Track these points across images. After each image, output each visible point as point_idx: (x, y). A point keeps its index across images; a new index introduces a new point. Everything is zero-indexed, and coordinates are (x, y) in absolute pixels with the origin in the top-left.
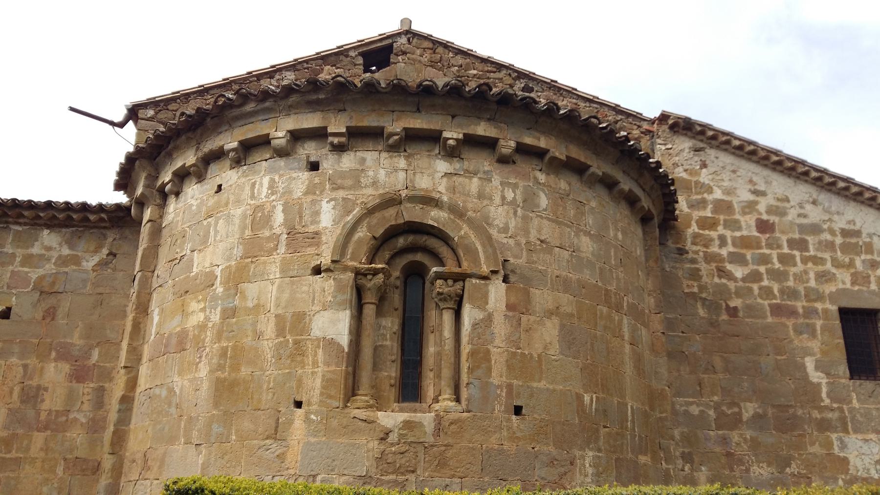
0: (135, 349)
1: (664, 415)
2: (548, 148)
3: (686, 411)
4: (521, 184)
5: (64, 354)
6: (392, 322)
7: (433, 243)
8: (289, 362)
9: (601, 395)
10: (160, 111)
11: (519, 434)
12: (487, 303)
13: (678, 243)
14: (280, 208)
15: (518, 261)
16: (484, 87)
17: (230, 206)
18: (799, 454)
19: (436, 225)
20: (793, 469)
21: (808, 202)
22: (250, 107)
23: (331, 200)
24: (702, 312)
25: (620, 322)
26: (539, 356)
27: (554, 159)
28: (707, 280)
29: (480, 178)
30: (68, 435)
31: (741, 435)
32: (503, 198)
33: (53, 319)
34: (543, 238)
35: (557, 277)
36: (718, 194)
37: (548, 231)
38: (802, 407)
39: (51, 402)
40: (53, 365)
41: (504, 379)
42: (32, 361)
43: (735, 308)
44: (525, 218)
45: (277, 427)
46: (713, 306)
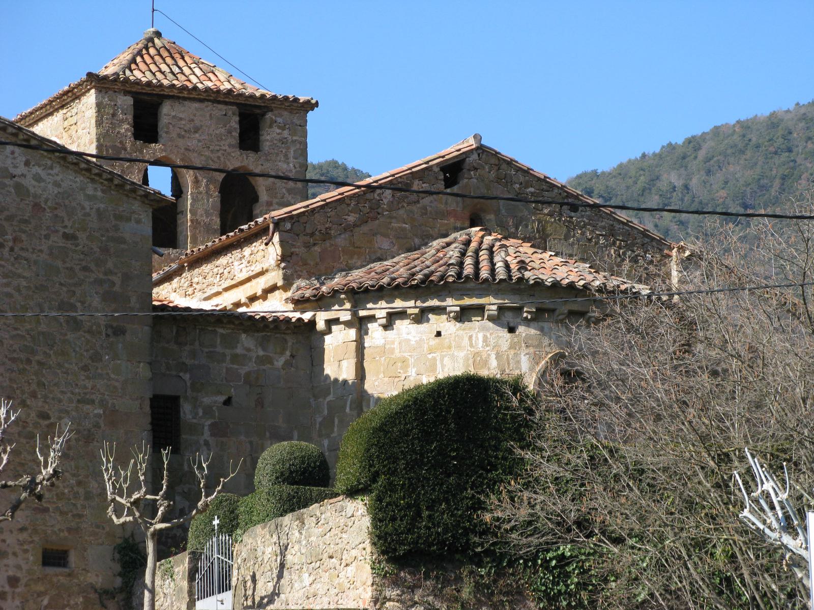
14: (493, 356)
17: (453, 349)
23: (527, 354)
33: (262, 407)
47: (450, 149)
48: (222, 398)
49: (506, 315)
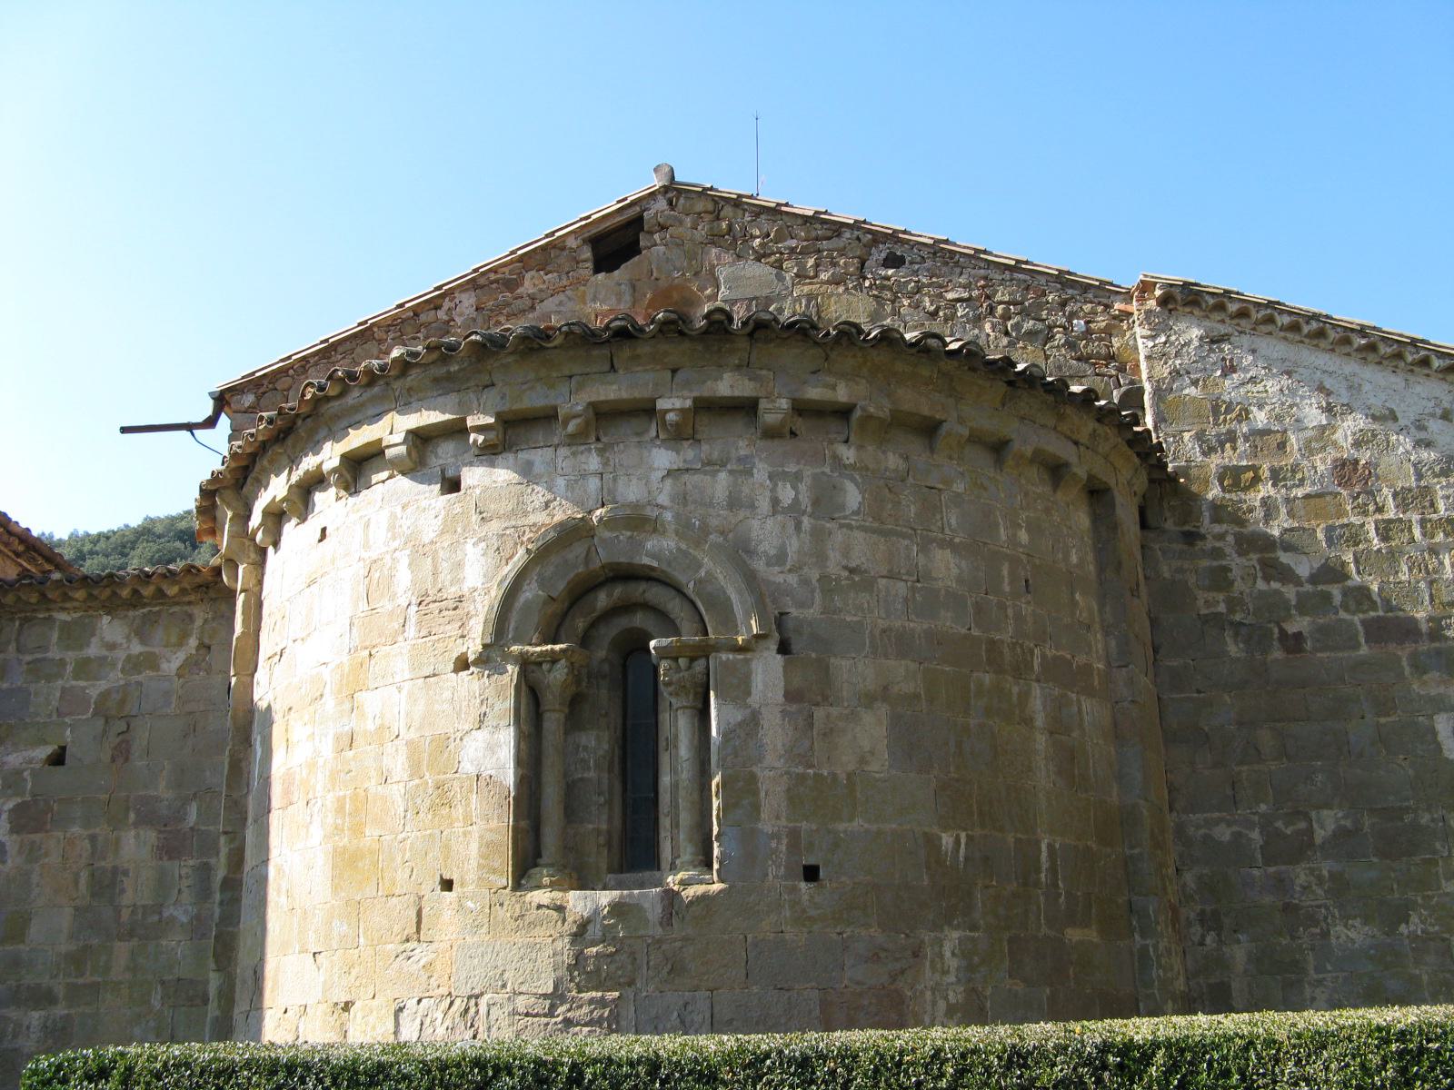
0: (236, 803)
1: (1136, 851)
2: (853, 400)
3: (1207, 838)
4: (808, 472)
5: (147, 818)
6: (598, 738)
7: (655, 594)
8: (430, 817)
9: (977, 832)
10: (264, 393)
11: (812, 912)
12: (749, 694)
13: (1185, 523)
15: (807, 613)
16: (718, 317)
18: (1424, 898)
19: (655, 564)
20: (1414, 925)
21: (1433, 415)
22: (354, 397)
23: (481, 540)
24: (1234, 649)
25: (1025, 696)
26: (849, 776)
27: (869, 417)
28: (1243, 588)
29: (731, 472)
30: (164, 943)
31: (1312, 871)
32: (775, 502)
33: (127, 759)
34: (853, 564)
35: (884, 631)
36: (1260, 418)
37: (862, 549)
38: (1429, 809)
39: (135, 893)
40: (133, 833)
41: (783, 822)
42: (102, 830)
43: (1298, 636)
44: (819, 535)
45: (419, 923)
46: (1255, 637)
47: (601, 197)
48: (43, 752)
49: (440, 451)
